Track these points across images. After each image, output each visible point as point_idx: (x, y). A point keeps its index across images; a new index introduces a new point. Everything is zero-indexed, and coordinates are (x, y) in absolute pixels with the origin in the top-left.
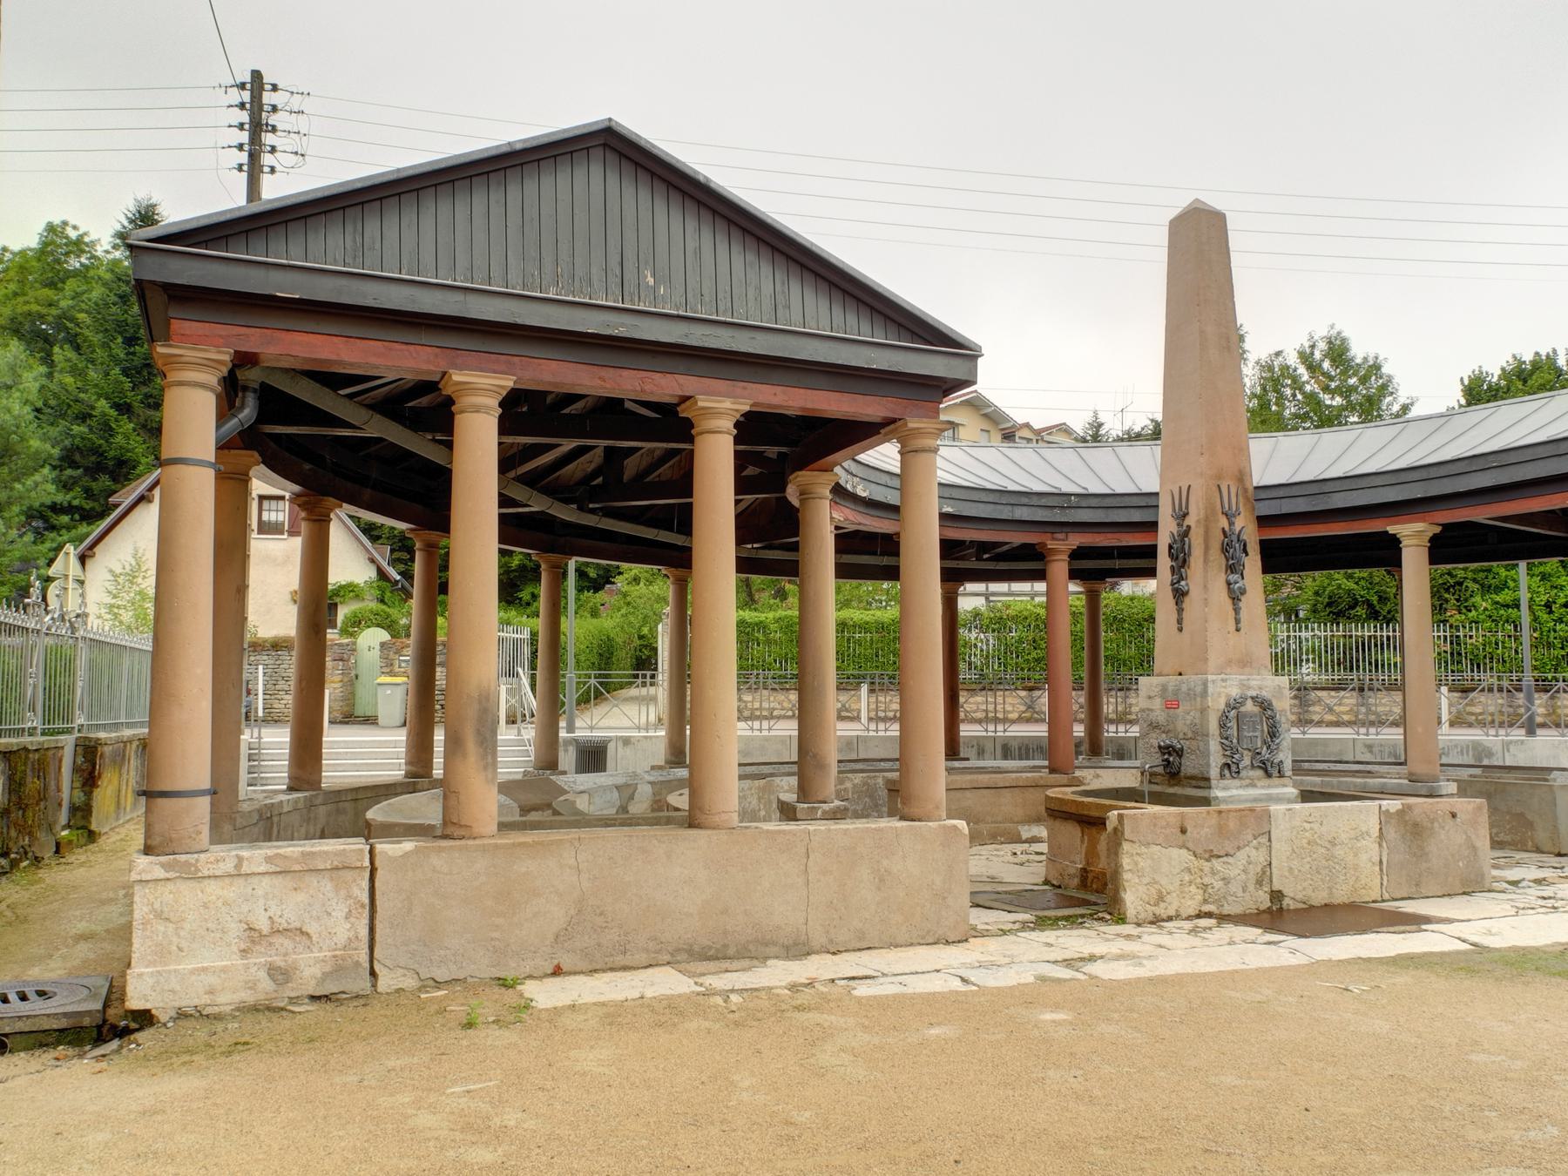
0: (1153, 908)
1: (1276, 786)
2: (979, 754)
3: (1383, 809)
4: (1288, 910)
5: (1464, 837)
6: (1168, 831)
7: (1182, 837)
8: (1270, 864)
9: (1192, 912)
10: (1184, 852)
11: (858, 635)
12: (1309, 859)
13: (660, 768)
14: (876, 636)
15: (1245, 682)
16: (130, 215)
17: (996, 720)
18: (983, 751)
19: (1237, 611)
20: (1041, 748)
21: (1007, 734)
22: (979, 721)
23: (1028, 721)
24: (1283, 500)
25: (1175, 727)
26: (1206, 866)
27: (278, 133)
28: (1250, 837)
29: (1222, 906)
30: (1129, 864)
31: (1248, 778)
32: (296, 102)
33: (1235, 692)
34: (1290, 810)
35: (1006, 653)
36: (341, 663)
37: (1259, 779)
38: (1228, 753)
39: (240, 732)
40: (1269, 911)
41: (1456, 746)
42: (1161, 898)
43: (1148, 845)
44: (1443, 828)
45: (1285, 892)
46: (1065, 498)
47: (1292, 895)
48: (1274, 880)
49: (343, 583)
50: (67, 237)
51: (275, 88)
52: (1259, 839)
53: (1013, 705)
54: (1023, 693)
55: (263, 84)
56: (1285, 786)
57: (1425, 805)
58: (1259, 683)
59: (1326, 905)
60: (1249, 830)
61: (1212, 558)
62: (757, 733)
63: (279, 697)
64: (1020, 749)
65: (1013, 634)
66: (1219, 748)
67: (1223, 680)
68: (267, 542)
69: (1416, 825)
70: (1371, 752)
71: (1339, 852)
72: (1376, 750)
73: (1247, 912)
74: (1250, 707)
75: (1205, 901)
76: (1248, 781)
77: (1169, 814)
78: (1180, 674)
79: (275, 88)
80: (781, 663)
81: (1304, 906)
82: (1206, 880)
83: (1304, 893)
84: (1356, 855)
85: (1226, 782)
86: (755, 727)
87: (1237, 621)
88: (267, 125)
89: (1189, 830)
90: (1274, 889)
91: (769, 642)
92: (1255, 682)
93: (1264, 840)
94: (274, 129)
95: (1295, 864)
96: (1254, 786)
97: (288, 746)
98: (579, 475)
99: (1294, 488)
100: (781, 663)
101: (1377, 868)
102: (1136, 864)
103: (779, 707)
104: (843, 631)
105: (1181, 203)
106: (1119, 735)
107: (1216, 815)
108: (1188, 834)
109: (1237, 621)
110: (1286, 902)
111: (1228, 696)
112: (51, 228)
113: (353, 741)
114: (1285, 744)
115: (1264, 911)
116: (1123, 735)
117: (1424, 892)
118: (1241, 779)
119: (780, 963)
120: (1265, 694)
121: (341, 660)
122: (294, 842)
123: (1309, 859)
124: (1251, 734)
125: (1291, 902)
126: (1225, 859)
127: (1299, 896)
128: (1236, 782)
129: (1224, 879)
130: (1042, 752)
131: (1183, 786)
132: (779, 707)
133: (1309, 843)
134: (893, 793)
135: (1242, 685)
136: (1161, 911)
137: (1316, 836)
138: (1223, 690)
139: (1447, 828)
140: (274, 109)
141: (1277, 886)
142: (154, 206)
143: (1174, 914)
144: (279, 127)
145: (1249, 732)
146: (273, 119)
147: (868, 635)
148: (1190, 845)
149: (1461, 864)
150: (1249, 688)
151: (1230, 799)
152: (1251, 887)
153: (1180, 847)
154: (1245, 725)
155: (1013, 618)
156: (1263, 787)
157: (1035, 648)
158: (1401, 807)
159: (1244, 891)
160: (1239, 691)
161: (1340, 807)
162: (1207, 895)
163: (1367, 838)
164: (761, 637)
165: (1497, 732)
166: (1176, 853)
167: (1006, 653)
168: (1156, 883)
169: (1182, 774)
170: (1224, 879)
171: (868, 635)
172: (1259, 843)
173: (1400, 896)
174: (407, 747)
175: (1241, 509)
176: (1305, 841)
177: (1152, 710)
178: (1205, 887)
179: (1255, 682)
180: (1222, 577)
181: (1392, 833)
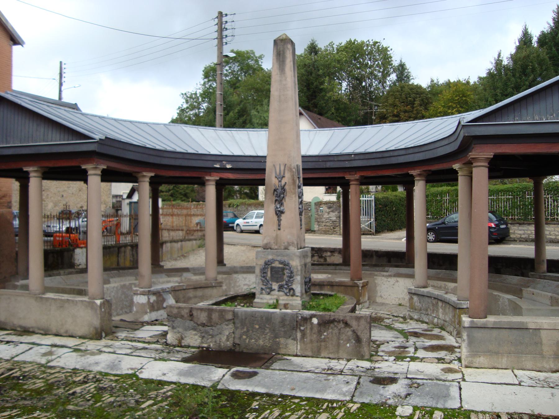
19: (279, 221)
24: (427, 152)
38: (265, 284)
51: (226, 15)
55: (222, 15)
94: (226, 29)
118: (272, 295)
140: (226, 22)
146: (227, 26)
180: (274, 205)
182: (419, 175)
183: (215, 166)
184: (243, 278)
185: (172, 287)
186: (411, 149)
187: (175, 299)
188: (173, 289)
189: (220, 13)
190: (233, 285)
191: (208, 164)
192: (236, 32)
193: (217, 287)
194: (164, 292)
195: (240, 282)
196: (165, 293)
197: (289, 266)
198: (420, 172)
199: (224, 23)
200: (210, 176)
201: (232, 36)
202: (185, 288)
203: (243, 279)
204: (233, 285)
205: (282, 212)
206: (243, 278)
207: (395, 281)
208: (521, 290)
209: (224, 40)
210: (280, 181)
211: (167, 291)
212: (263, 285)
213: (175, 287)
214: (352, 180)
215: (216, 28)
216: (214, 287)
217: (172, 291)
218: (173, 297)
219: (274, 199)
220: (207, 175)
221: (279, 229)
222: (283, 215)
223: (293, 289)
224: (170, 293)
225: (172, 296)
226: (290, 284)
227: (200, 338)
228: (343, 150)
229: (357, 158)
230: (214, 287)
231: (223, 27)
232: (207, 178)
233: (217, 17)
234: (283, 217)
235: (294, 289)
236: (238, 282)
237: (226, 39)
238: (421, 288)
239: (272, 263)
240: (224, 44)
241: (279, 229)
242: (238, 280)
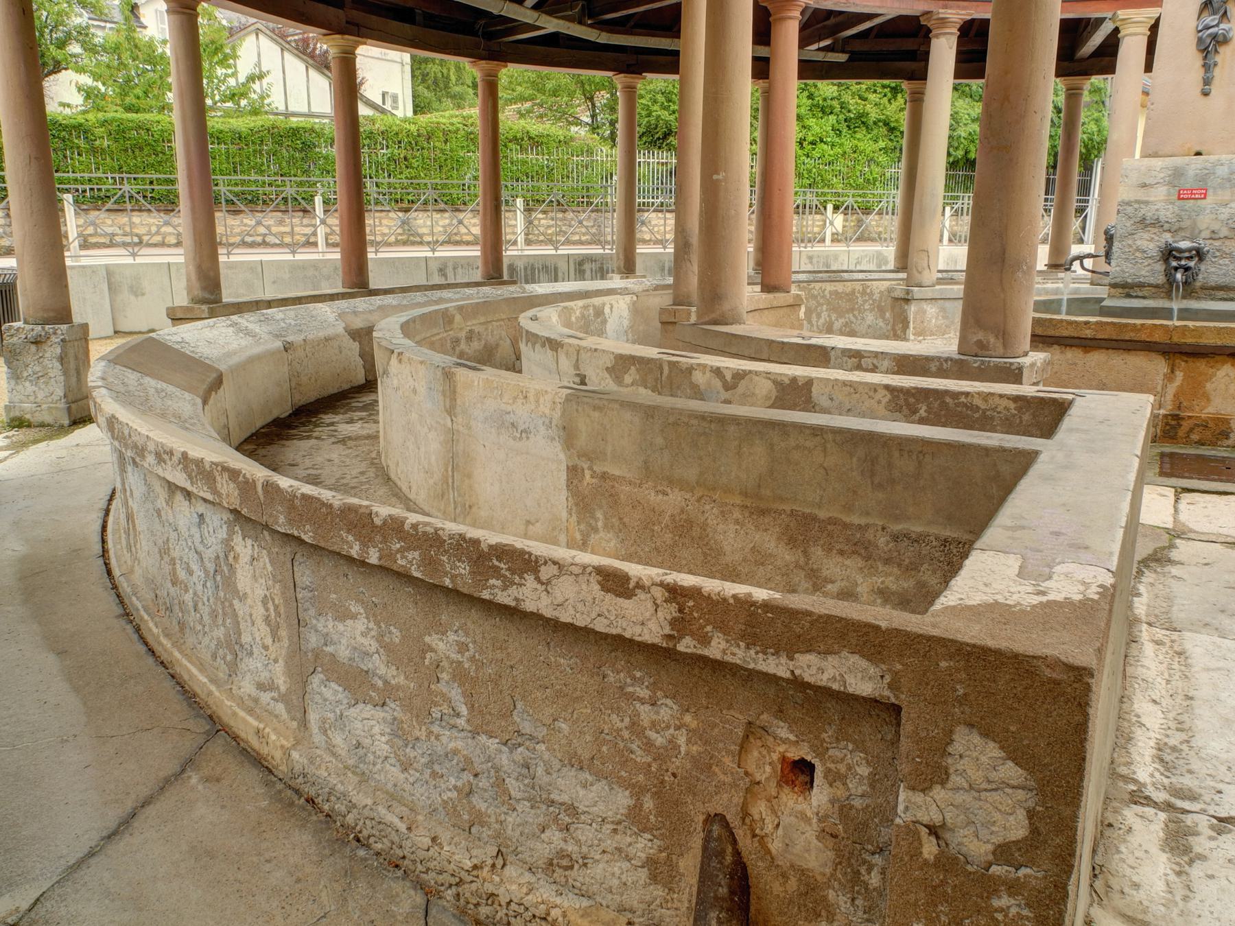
14: (233, 149)
20: (547, 267)
23: (405, 243)
25: (1195, 223)
35: (377, 171)
41: (866, 256)
53: (390, 227)
54: (400, 214)
64: (526, 269)
65: (384, 151)
70: (811, 263)
72: (815, 260)
78: (1198, 154)
91: (94, 151)
103: (120, 232)
122: (1076, 864)
130: (547, 272)
131: (1198, 298)
132: (120, 232)
134: (670, 327)
147: (223, 146)
157: (407, 167)
164: (81, 143)
167: (377, 171)
169: (1198, 284)
171: (223, 146)
177: (1147, 203)
222: (1221, 49)
241: (1206, 94)
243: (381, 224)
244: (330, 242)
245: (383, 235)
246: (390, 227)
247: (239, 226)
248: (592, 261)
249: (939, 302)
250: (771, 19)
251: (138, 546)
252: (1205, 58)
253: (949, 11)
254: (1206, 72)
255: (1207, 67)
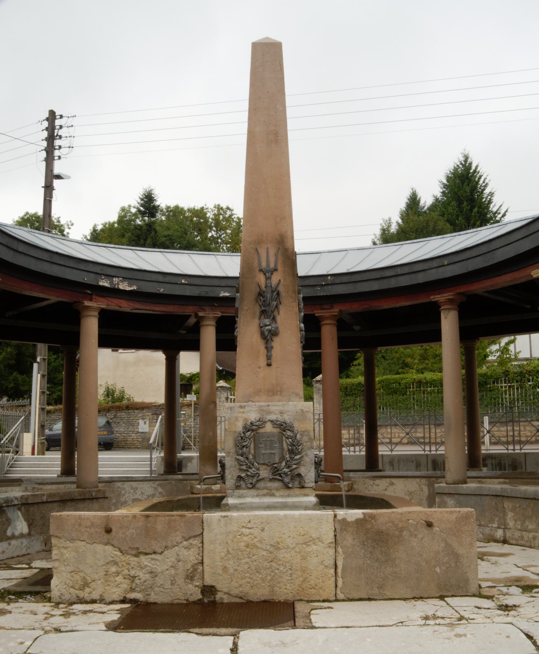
0: (78, 592)
1: (296, 496)
2: (417, 466)
3: (339, 518)
4: (222, 603)
5: (443, 545)
6: (92, 530)
7: (106, 536)
8: (202, 563)
9: (116, 597)
10: (109, 548)
11: (429, 389)
12: (247, 560)
13: (162, 475)
15: (265, 408)
16: (141, 197)
17: (514, 443)
18: (420, 465)
19: (269, 349)
21: (394, 453)
22: (503, 443)
24: (469, 261)
26: (133, 560)
27: (63, 139)
28: (179, 539)
29: (149, 595)
30: (56, 554)
31: (265, 488)
32: (70, 122)
33: (253, 416)
34: (224, 517)
36: (155, 416)
37: (277, 489)
38: (244, 467)
39: (325, 455)
40: (199, 602)
42: (86, 585)
43: (72, 540)
44: (416, 536)
45: (219, 586)
46: (322, 278)
47: (225, 590)
48: (205, 577)
49: (195, 373)
50: (131, 213)
51: (61, 117)
52: (191, 541)
53: (531, 432)
55: (56, 116)
56: (306, 495)
57: (393, 515)
58: (279, 408)
59: (265, 602)
60: (178, 533)
61: (246, 308)
62: (352, 453)
63: (130, 435)
66: (235, 463)
67: (241, 407)
68: (127, 354)
69: (380, 533)
71: (282, 555)
73: (176, 602)
74: (269, 428)
75: (132, 590)
76: (265, 491)
77: (420, 512)
79: (61, 117)
80: (383, 409)
81: (240, 601)
82: (133, 573)
83: (241, 589)
84: (304, 558)
85: (241, 491)
86: (351, 450)
87: (269, 358)
88: (57, 135)
89: (114, 530)
90: (206, 584)
92: (275, 408)
93: (196, 542)
94: (60, 137)
95: (231, 564)
96: (273, 495)
97: (60, 460)
98: (446, 306)
99: (475, 249)
100: (383, 409)
101: (332, 571)
102: (62, 555)
104: (420, 387)
105: (276, 37)
106: (516, 451)
107: (143, 519)
108: (113, 533)
109: (269, 358)
110: (219, 596)
111: (246, 420)
112: (123, 209)
113: (54, 458)
114: (307, 459)
115: (194, 603)
116: (519, 451)
117: (389, 594)
118: (258, 489)
119: (158, 602)
120: (287, 418)
121: (155, 414)
123: (247, 560)
124: (268, 451)
125: (225, 597)
126: (153, 556)
127: (235, 592)
128: (253, 492)
129: (151, 572)
133: (247, 546)
135: (261, 410)
136: (85, 594)
137: (255, 540)
138: (240, 415)
139: (420, 536)
140: (61, 127)
141: (209, 581)
142: (151, 190)
143: (98, 598)
144: (63, 135)
145: (266, 449)
146: (61, 132)
148: (115, 542)
149: (438, 570)
150: (269, 413)
151: (240, 506)
152: (180, 581)
153: (106, 544)
154: (261, 444)
155: (530, 372)
156: (282, 496)
158: (361, 516)
159: (172, 584)
160: (258, 415)
161: (285, 516)
162: (134, 585)
163: (320, 543)
165: (514, 447)
166: (100, 548)
167: (526, 396)
168: (80, 571)
170: (151, 572)
172: (191, 544)
173: (357, 597)
174: (62, 461)
175: (280, 268)
176: (243, 544)
178: (133, 578)
179: (275, 408)
180: (256, 322)
181: (349, 540)
182: (450, 301)
183: (101, 284)
184: (132, 488)
185: (22, 497)
186: (438, 260)
187: (26, 520)
188: (24, 502)
189: (52, 113)
190: (114, 501)
191: (87, 279)
192: (75, 142)
193: (100, 500)
194: (8, 506)
195: (126, 495)
196: (11, 509)
197: (292, 431)
198: (453, 295)
199: (58, 127)
200: (91, 300)
201: (69, 147)
202: (45, 499)
203: (132, 491)
204: (114, 501)
205: (274, 333)
206: (132, 488)
207: (387, 484)
208: (202, 593)
209: (57, 153)
210: (268, 278)
211: (15, 505)
212: (241, 470)
213: (27, 498)
214: (327, 318)
215: (45, 134)
216: (93, 499)
217: (23, 504)
218: (24, 515)
219: (258, 310)
220: (85, 299)
221: (269, 365)
222: (275, 339)
223: (299, 475)
224: (19, 509)
225: (22, 514)
226: (294, 466)
227: (127, 581)
228: (307, 273)
229: (338, 280)
230: (93, 499)
231: (55, 134)
232: (87, 303)
233: (47, 119)
234: (276, 343)
235: (303, 475)
236: (124, 495)
237: (61, 150)
238: (458, 484)
239: (259, 427)
240: (56, 158)
241: (269, 365)
242: (123, 492)
243: (525, 430)
244: (493, 441)
245: (527, 436)
246: (531, 432)
247: (440, 432)
248: (492, 458)
249: (456, 496)
250: (320, 324)
251: (437, 627)
252: (267, 343)
253: (437, 296)
254: (267, 352)
255: (269, 349)
